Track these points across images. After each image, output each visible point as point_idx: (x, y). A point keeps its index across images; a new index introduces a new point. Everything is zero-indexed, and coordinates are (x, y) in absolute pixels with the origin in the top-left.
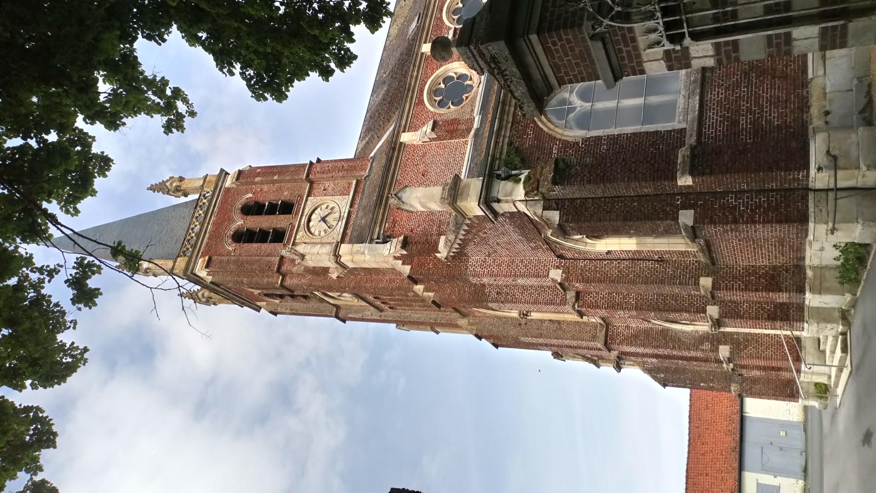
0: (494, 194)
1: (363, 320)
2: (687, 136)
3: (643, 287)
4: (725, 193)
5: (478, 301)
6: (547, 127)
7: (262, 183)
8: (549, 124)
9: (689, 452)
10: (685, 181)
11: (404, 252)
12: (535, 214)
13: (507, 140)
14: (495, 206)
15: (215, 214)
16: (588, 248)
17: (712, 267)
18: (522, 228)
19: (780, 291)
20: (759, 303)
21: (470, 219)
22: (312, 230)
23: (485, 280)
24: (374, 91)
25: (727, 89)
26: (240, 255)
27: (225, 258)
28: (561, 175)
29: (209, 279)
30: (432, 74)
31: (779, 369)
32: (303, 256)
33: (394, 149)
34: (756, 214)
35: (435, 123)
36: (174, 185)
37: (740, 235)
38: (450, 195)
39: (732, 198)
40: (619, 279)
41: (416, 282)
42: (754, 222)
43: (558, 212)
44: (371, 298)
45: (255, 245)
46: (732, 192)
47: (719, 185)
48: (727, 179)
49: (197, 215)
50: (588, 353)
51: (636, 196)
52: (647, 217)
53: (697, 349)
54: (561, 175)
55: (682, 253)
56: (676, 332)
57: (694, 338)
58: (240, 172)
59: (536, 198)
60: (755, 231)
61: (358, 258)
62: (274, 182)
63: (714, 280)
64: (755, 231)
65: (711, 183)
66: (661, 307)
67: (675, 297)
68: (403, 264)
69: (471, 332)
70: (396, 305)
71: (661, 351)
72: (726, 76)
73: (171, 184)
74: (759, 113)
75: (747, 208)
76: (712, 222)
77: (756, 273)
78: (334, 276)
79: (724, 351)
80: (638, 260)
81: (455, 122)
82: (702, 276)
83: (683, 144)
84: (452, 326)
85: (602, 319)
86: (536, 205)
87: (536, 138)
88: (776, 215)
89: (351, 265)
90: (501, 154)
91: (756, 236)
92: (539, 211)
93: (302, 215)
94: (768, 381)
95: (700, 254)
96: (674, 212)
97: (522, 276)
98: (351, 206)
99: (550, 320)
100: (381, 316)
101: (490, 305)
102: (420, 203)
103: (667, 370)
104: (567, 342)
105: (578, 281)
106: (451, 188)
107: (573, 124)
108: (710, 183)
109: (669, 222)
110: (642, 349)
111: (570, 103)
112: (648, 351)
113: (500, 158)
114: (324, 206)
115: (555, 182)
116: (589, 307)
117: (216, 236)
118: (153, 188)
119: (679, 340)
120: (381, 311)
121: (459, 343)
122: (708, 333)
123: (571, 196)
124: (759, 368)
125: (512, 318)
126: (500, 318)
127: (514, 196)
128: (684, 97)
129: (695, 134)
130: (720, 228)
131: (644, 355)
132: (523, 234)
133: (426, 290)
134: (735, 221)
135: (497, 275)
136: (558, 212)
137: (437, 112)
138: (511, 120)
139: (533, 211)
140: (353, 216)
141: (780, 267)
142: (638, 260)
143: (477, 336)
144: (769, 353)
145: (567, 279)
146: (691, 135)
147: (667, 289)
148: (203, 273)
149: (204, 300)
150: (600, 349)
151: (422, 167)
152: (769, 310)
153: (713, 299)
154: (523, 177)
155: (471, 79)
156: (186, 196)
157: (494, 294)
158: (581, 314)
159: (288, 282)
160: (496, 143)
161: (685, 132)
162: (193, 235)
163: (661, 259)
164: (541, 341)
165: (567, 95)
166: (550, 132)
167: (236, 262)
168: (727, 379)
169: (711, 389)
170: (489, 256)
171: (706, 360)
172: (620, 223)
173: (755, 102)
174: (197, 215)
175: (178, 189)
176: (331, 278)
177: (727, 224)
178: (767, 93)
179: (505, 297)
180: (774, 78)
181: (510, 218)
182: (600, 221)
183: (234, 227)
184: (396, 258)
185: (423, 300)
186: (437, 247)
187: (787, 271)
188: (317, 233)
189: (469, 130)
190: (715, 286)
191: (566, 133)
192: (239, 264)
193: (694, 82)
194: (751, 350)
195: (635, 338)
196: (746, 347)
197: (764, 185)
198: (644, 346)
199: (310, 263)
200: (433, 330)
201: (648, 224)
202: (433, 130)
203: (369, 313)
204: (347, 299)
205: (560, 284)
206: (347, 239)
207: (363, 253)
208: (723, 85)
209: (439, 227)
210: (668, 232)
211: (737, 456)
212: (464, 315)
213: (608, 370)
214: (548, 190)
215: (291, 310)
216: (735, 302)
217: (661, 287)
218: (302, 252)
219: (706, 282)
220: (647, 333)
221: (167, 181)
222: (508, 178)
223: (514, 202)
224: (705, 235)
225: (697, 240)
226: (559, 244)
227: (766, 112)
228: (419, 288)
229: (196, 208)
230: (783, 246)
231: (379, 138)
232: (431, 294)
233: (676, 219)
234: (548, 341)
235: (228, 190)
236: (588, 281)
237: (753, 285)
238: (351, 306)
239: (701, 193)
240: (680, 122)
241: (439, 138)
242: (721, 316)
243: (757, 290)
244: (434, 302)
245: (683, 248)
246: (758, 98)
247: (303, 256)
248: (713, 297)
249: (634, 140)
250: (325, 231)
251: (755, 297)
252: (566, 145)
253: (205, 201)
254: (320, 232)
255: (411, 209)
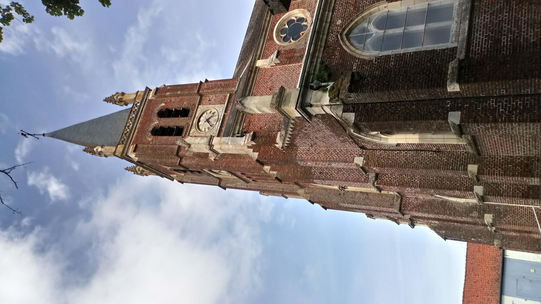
0: (308, 100)
1: (236, 188)
2: (458, 53)
3: (424, 171)
4: (487, 98)
5: (306, 178)
6: (350, 49)
7: (171, 96)
8: (351, 47)
9: (465, 280)
10: (454, 88)
11: (254, 143)
12: (337, 115)
13: (320, 60)
14: (309, 109)
15: (142, 117)
16: (382, 142)
17: (478, 156)
18: (332, 126)
19: (533, 176)
20: (515, 185)
21: (293, 119)
22: (201, 128)
23: (309, 164)
24: (247, 34)
25: (492, 14)
26: (155, 144)
27: (146, 146)
28: (356, 84)
29: (136, 159)
30: (280, 18)
31: (530, 232)
32: (189, 145)
33: (251, 71)
34: (513, 114)
35: (279, 53)
36: (119, 97)
37: (499, 132)
38: (276, 102)
39: (493, 102)
40: (406, 165)
41: (263, 164)
42: (511, 121)
43: (354, 114)
44: (239, 174)
45: (165, 137)
46: (493, 97)
47: (482, 91)
48: (488, 85)
49: (131, 117)
50: (392, 216)
51: (415, 101)
52: (424, 117)
53: (468, 216)
54: (356, 84)
55: (454, 146)
56: (452, 203)
57: (466, 208)
58: (157, 89)
59: (338, 103)
60: (512, 129)
61: (225, 147)
62: (178, 96)
63: (479, 167)
64: (512, 129)
65: (475, 90)
66: (439, 186)
67: (450, 179)
68: (254, 151)
69: (306, 199)
70: (257, 179)
71: (441, 217)
72: (492, 4)
73: (117, 97)
74: (517, 33)
75: (506, 110)
76: (476, 121)
77: (514, 162)
78: (212, 159)
79: (488, 218)
80: (421, 150)
81: (292, 51)
82: (470, 163)
83: (453, 58)
84: (295, 194)
85: (398, 193)
86: (337, 108)
87: (341, 58)
88: (530, 116)
89: (221, 152)
90: (315, 70)
91: (513, 133)
92: (340, 113)
93: (194, 118)
94: (523, 239)
95: (468, 146)
96: (444, 114)
97: (335, 161)
98: (225, 112)
99: (361, 192)
100: (247, 186)
101: (315, 181)
102: (257, 107)
103: (447, 228)
104: (373, 208)
105: (375, 165)
106: (278, 97)
107: (369, 46)
108: (475, 89)
109: (440, 121)
110: (427, 214)
111: (369, 31)
112: (431, 216)
113: (314, 74)
114: (209, 112)
115: (350, 90)
116: (385, 184)
117: (142, 131)
118: (107, 100)
119: (455, 209)
120: (248, 182)
121: (298, 204)
122: (476, 205)
123: (364, 101)
124: (515, 231)
125: (334, 190)
126: (326, 189)
127: (322, 102)
128: (457, 22)
129: (464, 51)
130: (482, 126)
131: (428, 219)
132: (333, 131)
133: (272, 169)
134: (495, 121)
135: (317, 160)
136: (354, 114)
137: (282, 44)
138: (323, 45)
139: (337, 113)
140: (227, 118)
141: (533, 158)
142: (421, 150)
143: (310, 201)
144: (523, 221)
145: (367, 164)
146: (461, 52)
147: (442, 173)
148: (133, 156)
149: (139, 172)
150: (396, 213)
151: (269, 84)
152: (523, 190)
153: (478, 181)
154: (329, 87)
155: (306, 21)
156: (126, 105)
157: (317, 174)
158: (380, 190)
159: (184, 162)
160: (312, 62)
161: (456, 50)
162: (128, 130)
163: (438, 150)
164: (354, 206)
165: (365, 25)
166: (352, 53)
167: (152, 148)
168: (491, 237)
169: (480, 242)
170: (312, 146)
171: (475, 224)
172: (401, 122)
173: (515, 24)
174: (131, 117)
175: (121, 101)
176: (210, 160)
177: (488, 122)
178: (525, 17)
179: (325, 176)
180: (531, 4)
181: (322, 119)
182: (386, 120)
183: (153, 125)
184: (249, 147)
185: (269, 176)
186: (276, 140)
187: (538, 161)
188: (203, 130)
189: (302, 57)
190: (480, 172)
191: (363, 53)
192: (154, 150)
193: (465, 10)
194: (509, 218)
195: (421, 206)
196: (505, 216)
197: (521, 90)
198: (428, 212)
199: (195, 149)
200: (283, 196)
201: (424, 123)
202: (277, 57)
203: (240, 184)
204: (224, 174)
205: (362, 168)
206: (222, 134)
207: (227, 144)
208: (488, 11)
209: (279, 126)
210: (439, 130)
211: (499, 285)
212: (302, 187)
213: (405, 226)
214: (345, 97)
215: (192, 180)
216: (496, 184)
217: (439, 171)
218: (188, 142)
219: (473, 168)
220: (431, 203)
221: (115, 95)
222: (318, 88)
223: (322, 106)
224: (470, 132)
225: (463, 136)
226: (360, 138)
227: (524, 31)
228: (267, 168)
229: (131, 113)
230: (535, 141)
231: (245, 65)
232: (275, 173)
233: (446, 119)
234: (364, 207)
235: (151, 101)
236: (382, 166)
237: (510, 171)
238: (229, 179)
239: (467, 98)
240: (452, 43)
241: (281, 63)
242: (485, 194)
243: (513, 175)
244: (277, 178)
245: (455, 142)
246: (517, 21)
247: (189, 145)
248: (478, 180)
249: (416, 58)
250: (208, 128)
251: (511, 180)
252: (363, 62)
253: (136, 108)
254: (205, 129)
255: (251, 112)
